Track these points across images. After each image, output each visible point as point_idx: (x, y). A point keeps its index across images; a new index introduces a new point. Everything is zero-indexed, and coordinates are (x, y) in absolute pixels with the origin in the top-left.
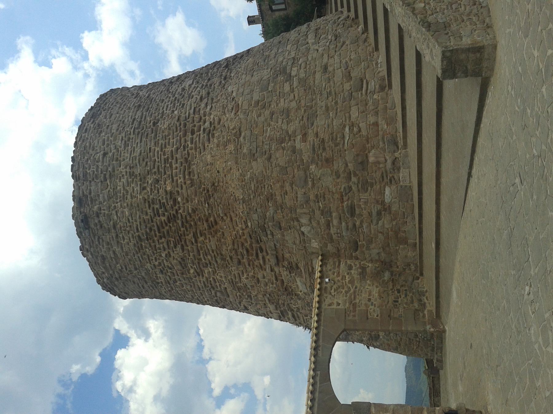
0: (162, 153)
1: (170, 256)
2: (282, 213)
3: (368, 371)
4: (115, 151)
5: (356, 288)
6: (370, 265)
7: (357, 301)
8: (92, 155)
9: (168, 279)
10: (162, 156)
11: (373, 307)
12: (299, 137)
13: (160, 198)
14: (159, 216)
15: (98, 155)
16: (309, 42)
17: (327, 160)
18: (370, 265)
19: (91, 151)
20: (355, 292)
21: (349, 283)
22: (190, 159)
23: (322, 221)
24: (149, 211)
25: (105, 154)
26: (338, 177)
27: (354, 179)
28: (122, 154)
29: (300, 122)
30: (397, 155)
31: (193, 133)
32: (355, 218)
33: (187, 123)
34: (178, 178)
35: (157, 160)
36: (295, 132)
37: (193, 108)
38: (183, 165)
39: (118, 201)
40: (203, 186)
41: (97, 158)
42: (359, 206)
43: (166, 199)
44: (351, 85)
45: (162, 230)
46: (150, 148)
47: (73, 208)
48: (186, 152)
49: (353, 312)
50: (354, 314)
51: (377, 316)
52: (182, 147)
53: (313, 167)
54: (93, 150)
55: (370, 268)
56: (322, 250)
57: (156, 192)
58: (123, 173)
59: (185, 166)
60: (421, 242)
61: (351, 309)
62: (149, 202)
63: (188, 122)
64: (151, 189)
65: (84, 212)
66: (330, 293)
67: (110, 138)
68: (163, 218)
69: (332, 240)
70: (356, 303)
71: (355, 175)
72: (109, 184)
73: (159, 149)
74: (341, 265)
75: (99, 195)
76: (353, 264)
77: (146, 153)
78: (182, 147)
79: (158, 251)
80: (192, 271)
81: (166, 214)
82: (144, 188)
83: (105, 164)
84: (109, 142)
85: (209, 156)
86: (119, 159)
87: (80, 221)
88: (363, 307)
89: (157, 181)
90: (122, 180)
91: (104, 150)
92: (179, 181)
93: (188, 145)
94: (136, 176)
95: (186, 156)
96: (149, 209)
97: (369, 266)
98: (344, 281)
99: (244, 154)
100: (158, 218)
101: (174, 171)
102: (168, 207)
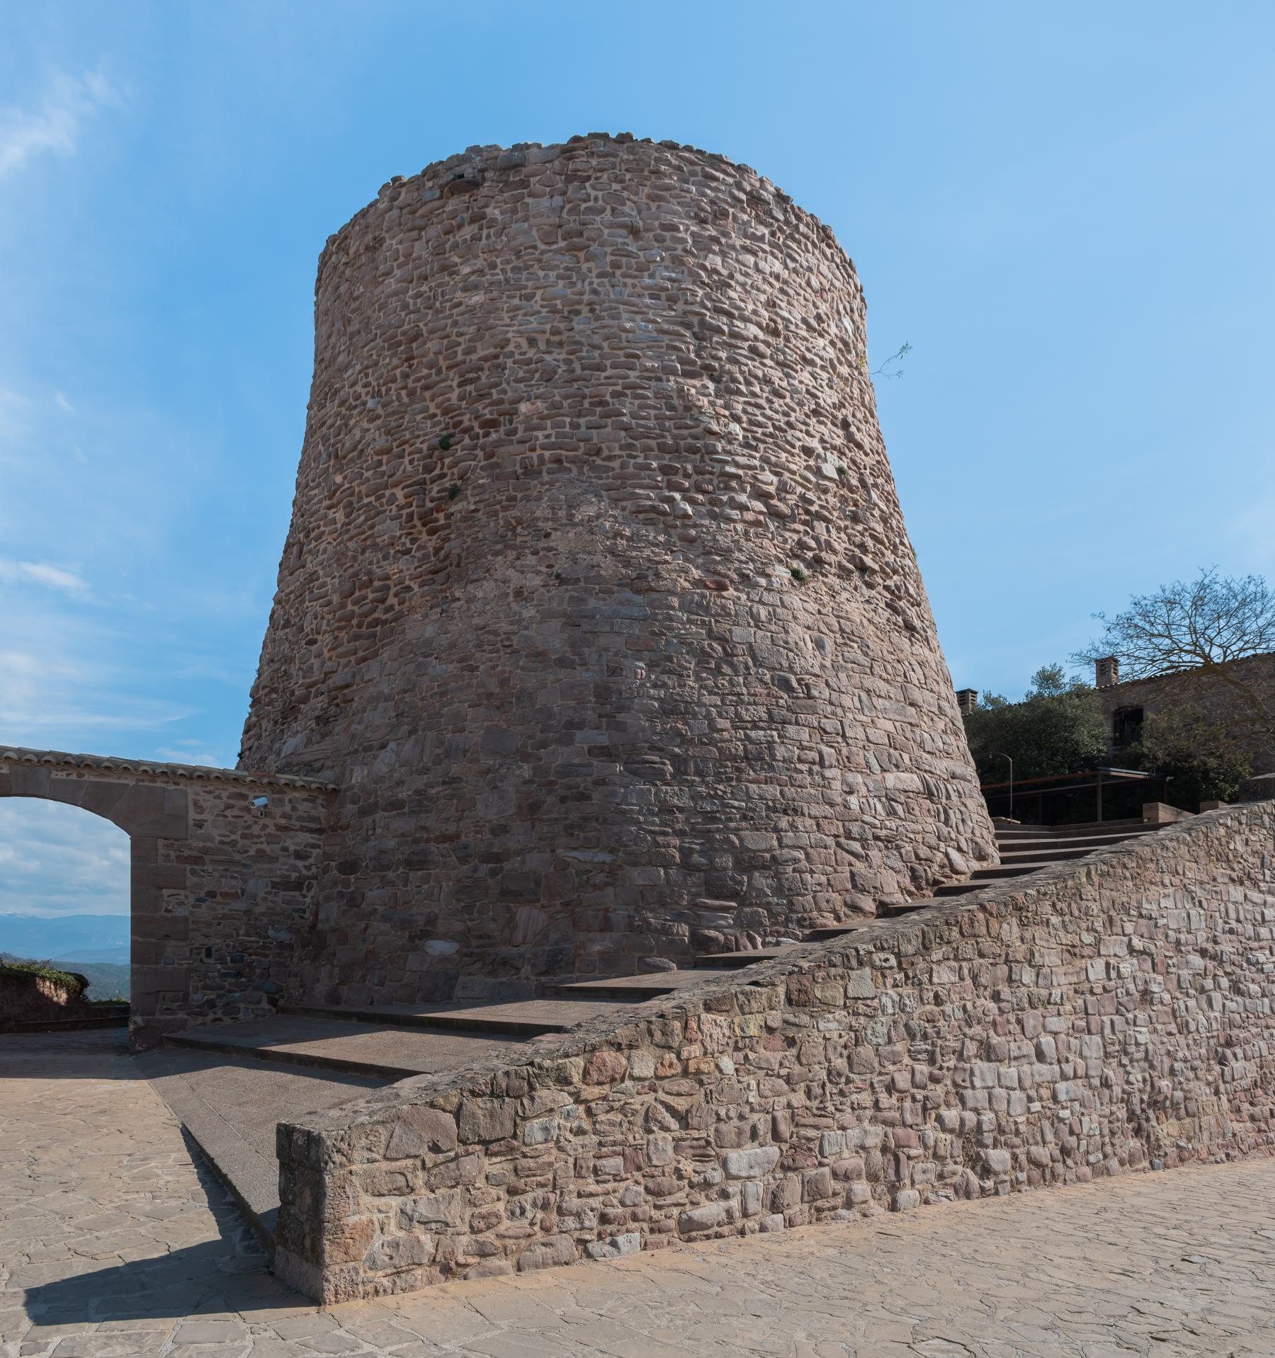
0: (619, 388)
1: (371, 421)
2: (432, 696)
3: (61, 889)
4: (642, 259)
5: (245, 866)
6: (308, 900)
7: (209, 867)
8: (636, 194)
9: (329, 422)
10: (610, 389)
11: (192, 900)
12: (603, 739)
13: (504, 385)
14: (460, 385)
15: (634, 213)
16: (887, 775)
17: (535, 807)
18: (308, 900)
19: (646, 190)
20: (233, 863)
21: (258, 851)
22: (599, 462)
23: (404, 793)
24: (474, 357)
25: (634, 232)
26: (494, 832)
27: (485, 868)
28: (629, 281)
29: (646, 742)
30: (526, 970)
31: (665, 470)
32: (401, 870)
33: (698, 456)
34: (549, 431)
35: (604, 374)
36: (621, 727)
37: (741, 472)
38: (582, 444)
39: (509, 274)
40: (519, 496)
41: (627, 209)
42: (426, 880)
43: (501, 402)
44: (725, 869)
45: (427, 394)
46: (637, 357)
47: (496, 147)
48: (617, 452)
49: (177, 857)
50: (173, 857)
51: (166, 910)
52: (630, 441)
53: (526, 771)
54: (649, 197)
55: (301, 899)
56: (346, 790)
57: (521, 374)
58: (579, 285)
59: (576, 450)
60: (339, 1015)
61: (186, 853)
62: (496, 357)
63: (702, 460)
64: (529, 362)
65: (484, 179)
66: (228, 807)
67: (680, 247)
68: (454, 396)
69: (364, 812)
70: (203, 864)
71: (493, 873)
72: (554, 247)
73: (632, 379)
74: (308, 835)
75: (526, 219)
76: (311, 861)
77: (625, 344)
78: (630, 441)
79: (383, 389)
80: (339, 479)
81: (463, 404)
82: (532, 342)
83: (606, 231)
84: (668, 243)
85: (591, 511)
86: (618, 273)
87: (458, 170)
88: (191, 880)
89: (548, 377)
90: (561, 283)
91: (647, 230)
92: (540, 434)
93: (635, 457)
94: (567, 319)
95: (606, 453)
96: (480, 359)
97: (305, 896)
98: (263, 839)
99: (582, 601)
100: (455, 384)
101: (568, 420)
102: (479, 406)
